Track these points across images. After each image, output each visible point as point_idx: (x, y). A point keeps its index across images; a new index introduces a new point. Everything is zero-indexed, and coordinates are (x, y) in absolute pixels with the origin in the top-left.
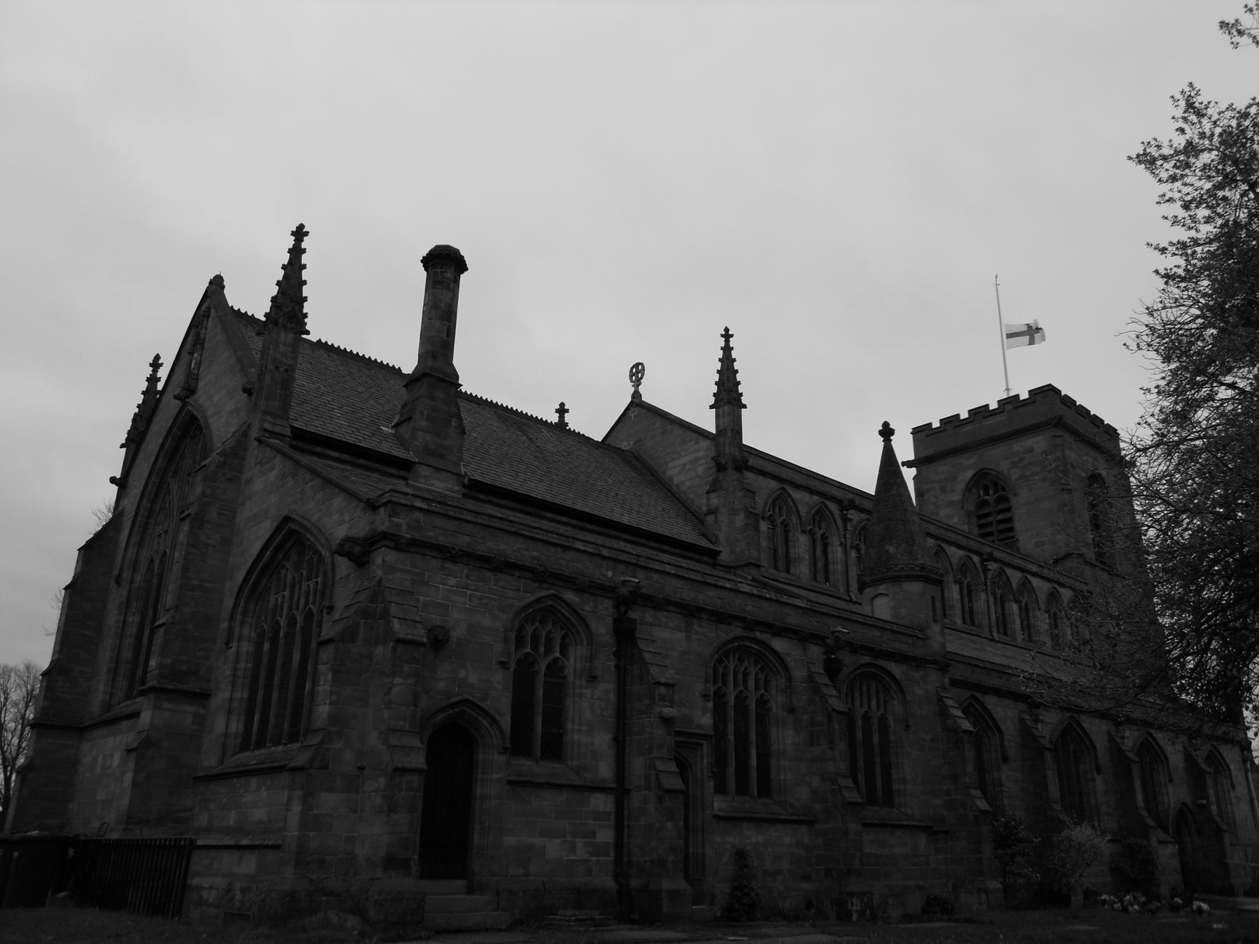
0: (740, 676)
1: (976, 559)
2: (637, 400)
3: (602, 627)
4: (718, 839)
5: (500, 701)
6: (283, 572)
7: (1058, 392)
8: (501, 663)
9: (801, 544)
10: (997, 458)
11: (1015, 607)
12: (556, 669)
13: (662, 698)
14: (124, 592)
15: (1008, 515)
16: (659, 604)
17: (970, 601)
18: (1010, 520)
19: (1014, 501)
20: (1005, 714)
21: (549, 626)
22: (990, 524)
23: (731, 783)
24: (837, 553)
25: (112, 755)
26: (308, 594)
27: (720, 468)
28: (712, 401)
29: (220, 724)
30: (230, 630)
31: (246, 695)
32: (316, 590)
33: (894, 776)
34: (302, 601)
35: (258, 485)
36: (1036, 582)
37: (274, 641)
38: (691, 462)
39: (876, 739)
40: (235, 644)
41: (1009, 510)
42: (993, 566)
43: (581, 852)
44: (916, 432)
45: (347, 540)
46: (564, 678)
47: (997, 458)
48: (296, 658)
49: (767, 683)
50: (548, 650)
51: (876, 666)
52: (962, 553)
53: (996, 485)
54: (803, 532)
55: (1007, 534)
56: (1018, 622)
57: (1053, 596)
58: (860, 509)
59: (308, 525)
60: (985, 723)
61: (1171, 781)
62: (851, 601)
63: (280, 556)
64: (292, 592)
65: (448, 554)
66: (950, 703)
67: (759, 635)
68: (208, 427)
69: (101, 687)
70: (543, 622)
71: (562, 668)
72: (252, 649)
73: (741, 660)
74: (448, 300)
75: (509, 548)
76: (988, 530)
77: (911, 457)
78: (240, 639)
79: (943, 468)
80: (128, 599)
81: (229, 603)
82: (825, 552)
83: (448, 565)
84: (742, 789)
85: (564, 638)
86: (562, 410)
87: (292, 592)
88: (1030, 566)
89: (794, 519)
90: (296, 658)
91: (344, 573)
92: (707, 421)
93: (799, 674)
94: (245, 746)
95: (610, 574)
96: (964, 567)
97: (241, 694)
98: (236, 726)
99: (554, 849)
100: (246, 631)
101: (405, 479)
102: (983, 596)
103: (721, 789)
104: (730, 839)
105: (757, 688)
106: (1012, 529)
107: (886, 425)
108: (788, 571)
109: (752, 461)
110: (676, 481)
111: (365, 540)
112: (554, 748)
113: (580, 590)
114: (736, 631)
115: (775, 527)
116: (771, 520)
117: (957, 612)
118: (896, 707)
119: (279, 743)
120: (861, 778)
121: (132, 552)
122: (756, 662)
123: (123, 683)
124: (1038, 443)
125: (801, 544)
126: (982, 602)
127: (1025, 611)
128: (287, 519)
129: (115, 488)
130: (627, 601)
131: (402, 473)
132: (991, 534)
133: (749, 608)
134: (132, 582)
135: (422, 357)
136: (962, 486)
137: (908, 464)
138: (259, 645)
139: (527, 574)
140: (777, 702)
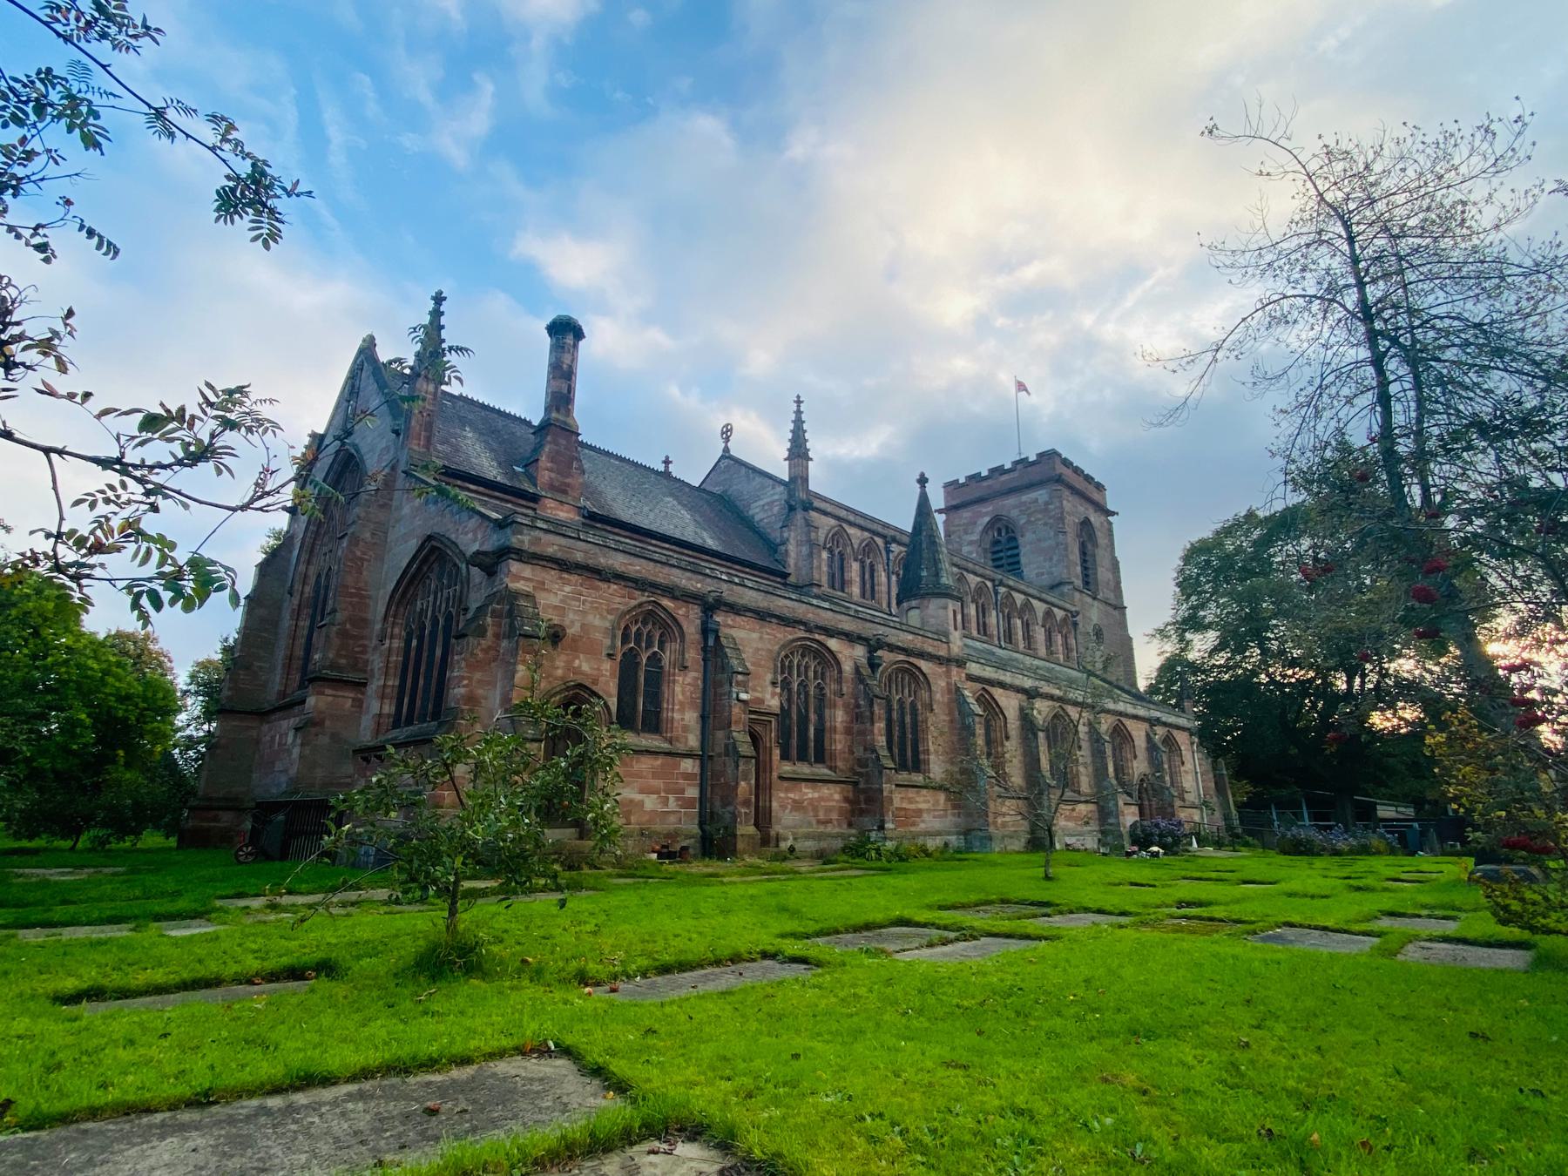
0: (802, 669)
1: (989, 584)
2: (726, 454)
3: (691, 627)
4: (782, 795)
5: (609, 689)
6: (428, 581)
7: (1060, 455)
8: (609, 655)
9: (854, 569)
10: (1009, 506)
11: (1019, 622)
12: (655, 659)
13: (738, 684)
14: (296, 601)
15: (1016, 551)
16: (735, 609)
17: (984, 616)
18: (1018, 555)
19: (1021, 541)
20: (1010, 704)
21: (650, 626)
22: (1001, 558)
23: (794, 752)
24: (882, 577)
25: (287, 734)
26: (448, 599)
27: (792, 509)
28: (786, 454)
29: (375, 707)
30: (383, 630)
31: (397, 683)
32: (454, 596)
33: (921, 749)
34: (444, 606)
35: (406, 510)
36: (1035, 602)
37: (421, 639)
38: (768, 504)
39: (908, 719)
40: (388, 641)
41: (1017, 547)
42: (1002, 590)
43: (672, 805)
44: (947, 485)
45: (478, 553)
46: (661, 667)
47: (1009, 506)
48: (438, 652)
49: (823, 674)
50: (649, 645)
51: (908, 663)
52: (979, 579)
53: (1007, 528)
54: (856, 560)
55: (1014, 567)
56: (1020, 633)
57: (1049, 614)
58: (900, 543)
59: (449, 544)
60: (993, 709)
61: (1135, 757)
62: (891, 615)
63: (425, 569)
64: (435, 599)
65: (563, 566)
66: (967, 693)
67: (817, 637)
68: (363, 461)
69: (278, 679)
70: (645, 623)
71: (660, 660)
72: (402, 645)
73: (803, 656)
74: (568, 362)
75: (618, 562)
76: (999, 563)
77: (943, 506)
78: (392, 637)
79: (966, 514)
80: (299, 605)
81: (381, 609)
82: (872, 577)
83: (565, 575)
84: (803, 757)
85: (661, 636)
86: (667, 462)
87: (435, 599)
88: (1031, 591)
89: (849, 550)
90: (438, 652)
91: (477, 581)
92: (782, 471)
93: (847, 667)
94: (396, 724)
95: (699, 585)
96: (980, 590)
97: (393, 682)
98: (389, 708)
99: (650, 803)
100: (396, 631)
101: (534, 510)
102: (994, 613)
103: (785, 756)
104: (792, 795)
105: (815, 678)
106: (1018, 562)
107: (922, 475)
108: (843, 591)
109: (817, 504)
110: (757, 518)
111: (493, 553)
112: (654, 723)
113: (674, 598)
114: (801, 633)
115: (833, 555)
116: (831, 551)
117: (974, 625)
118: (924, 695)
119: (425, 721)
120: (896, 751)
121: (302, 568)
122: (815, 658)
123: (297, 677)
124: (1041, 495)
125: (854, 569)
126: (992, 619)
127: (1027, 626)
128: (430, 538)
129: (287, 516)
130: (710, 606)
131: (532, 505)
132: (1002, 566)
133: (810, 615)
134: (302, 593)
135: (548, 410)
136: (981, 528)
137: (940, 511)
138: (408, 642)
139: (630, 584)
140: (830, 689)
